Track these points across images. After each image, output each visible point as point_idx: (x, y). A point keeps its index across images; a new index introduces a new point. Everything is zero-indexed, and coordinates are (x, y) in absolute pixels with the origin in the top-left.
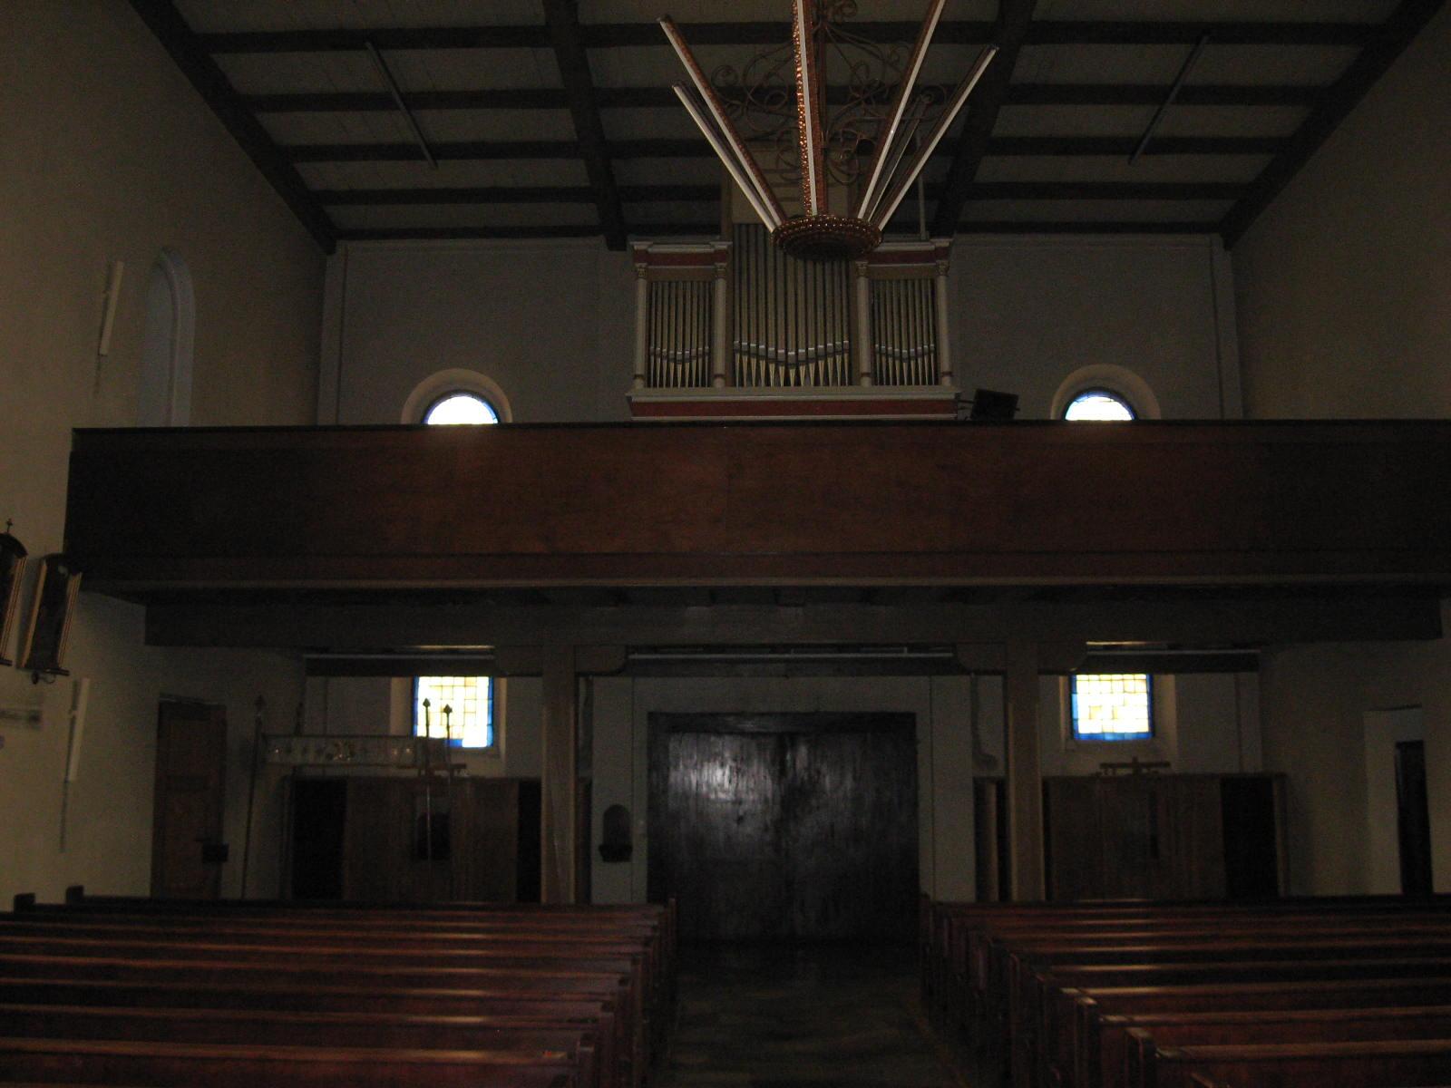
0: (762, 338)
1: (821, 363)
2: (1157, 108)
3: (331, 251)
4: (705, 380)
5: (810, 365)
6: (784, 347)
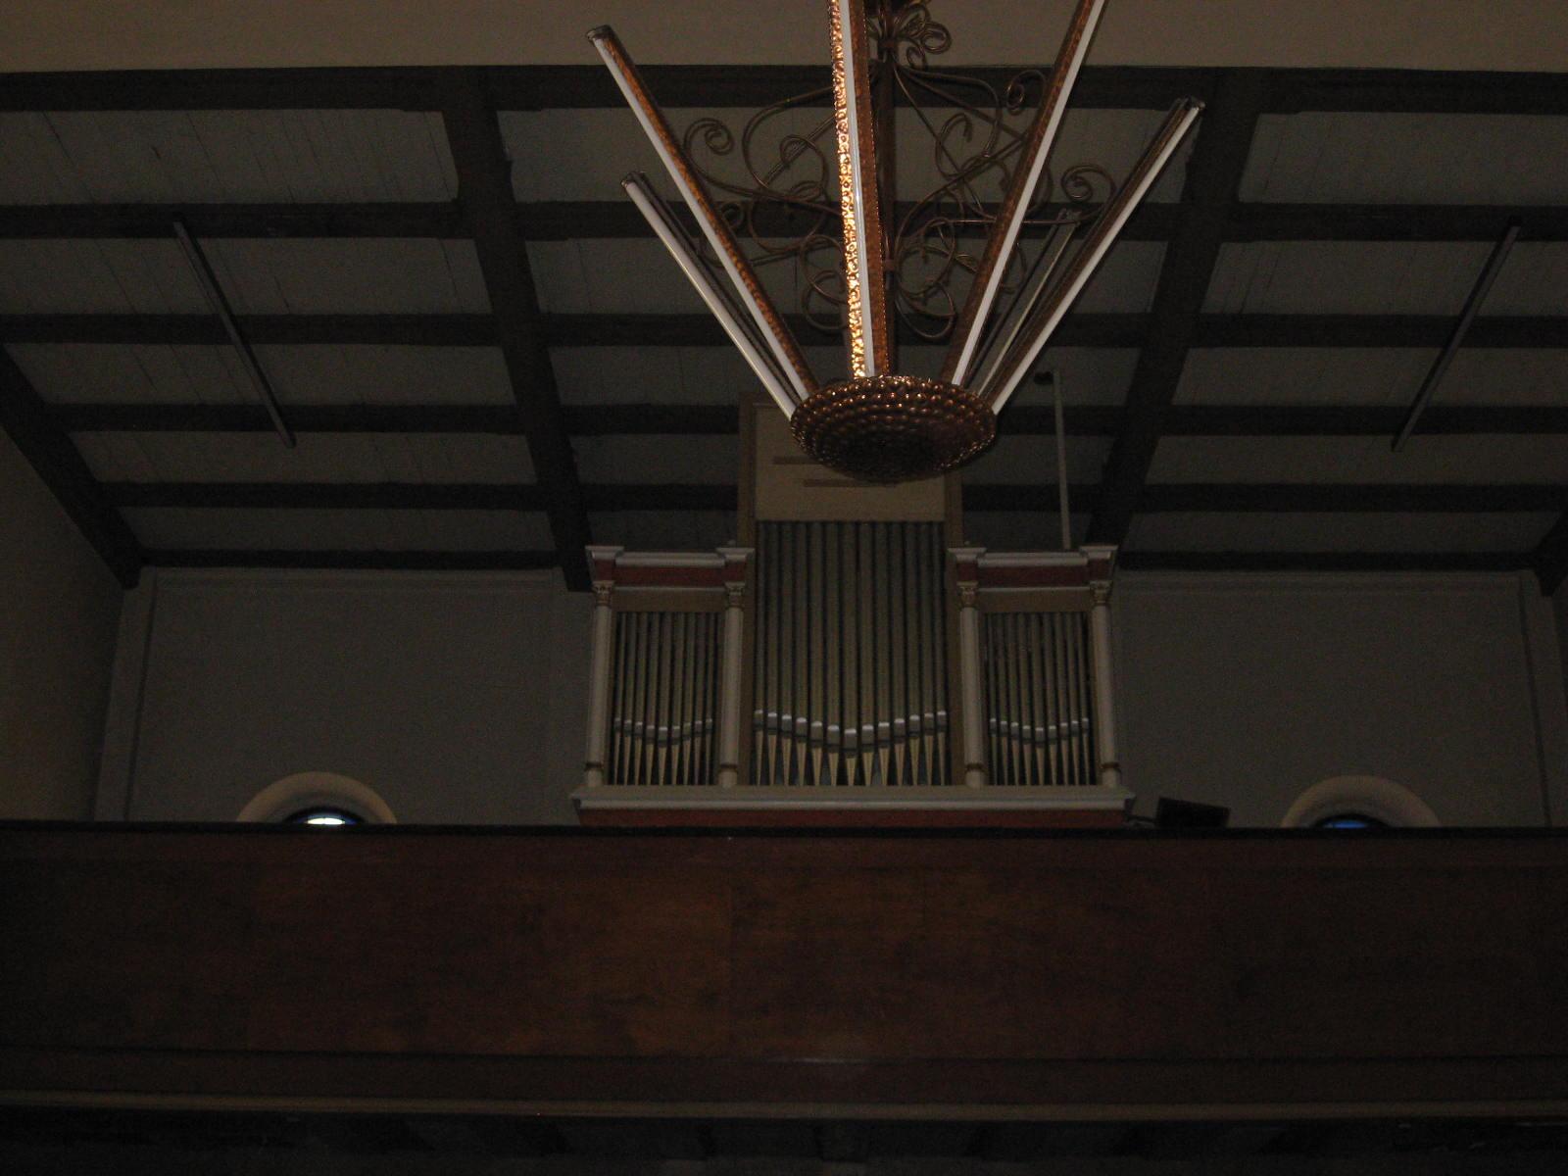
0: (802, 704)
1: (899, 749)
2: (1436, 352)
3: (132, 584)
4: (705, 773)
5: (881, 751)
6: (837, 721)
